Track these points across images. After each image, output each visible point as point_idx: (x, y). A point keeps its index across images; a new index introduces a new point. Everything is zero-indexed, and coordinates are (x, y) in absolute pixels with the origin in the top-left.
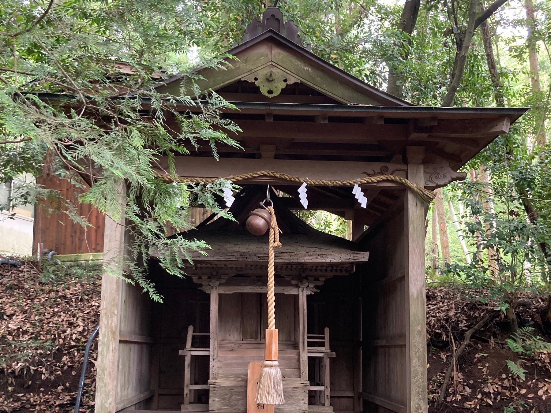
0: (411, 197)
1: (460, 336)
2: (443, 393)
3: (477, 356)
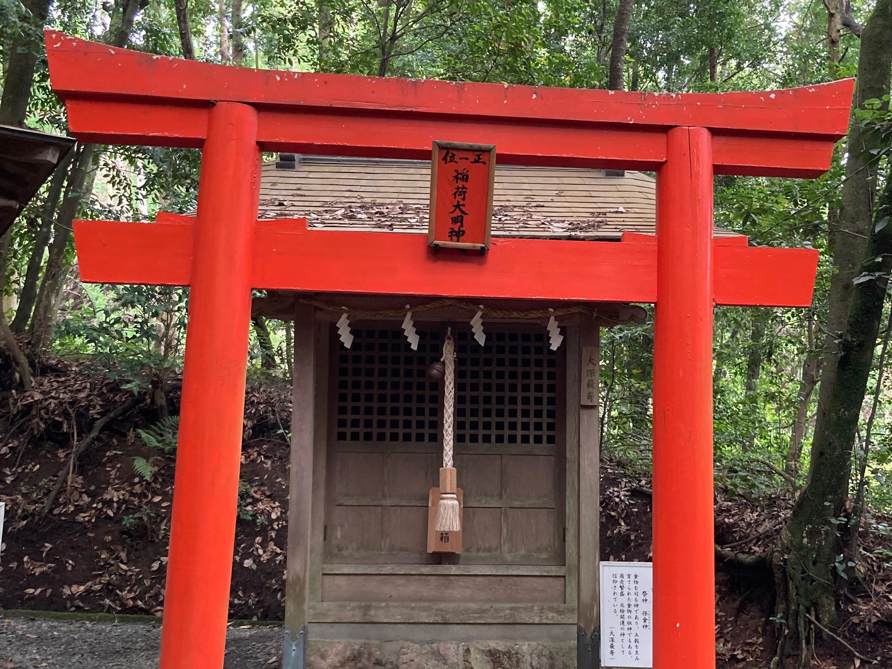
0: (859, 21)
1: (85, 425)
2: (50, 502)
3: (108, 454)
